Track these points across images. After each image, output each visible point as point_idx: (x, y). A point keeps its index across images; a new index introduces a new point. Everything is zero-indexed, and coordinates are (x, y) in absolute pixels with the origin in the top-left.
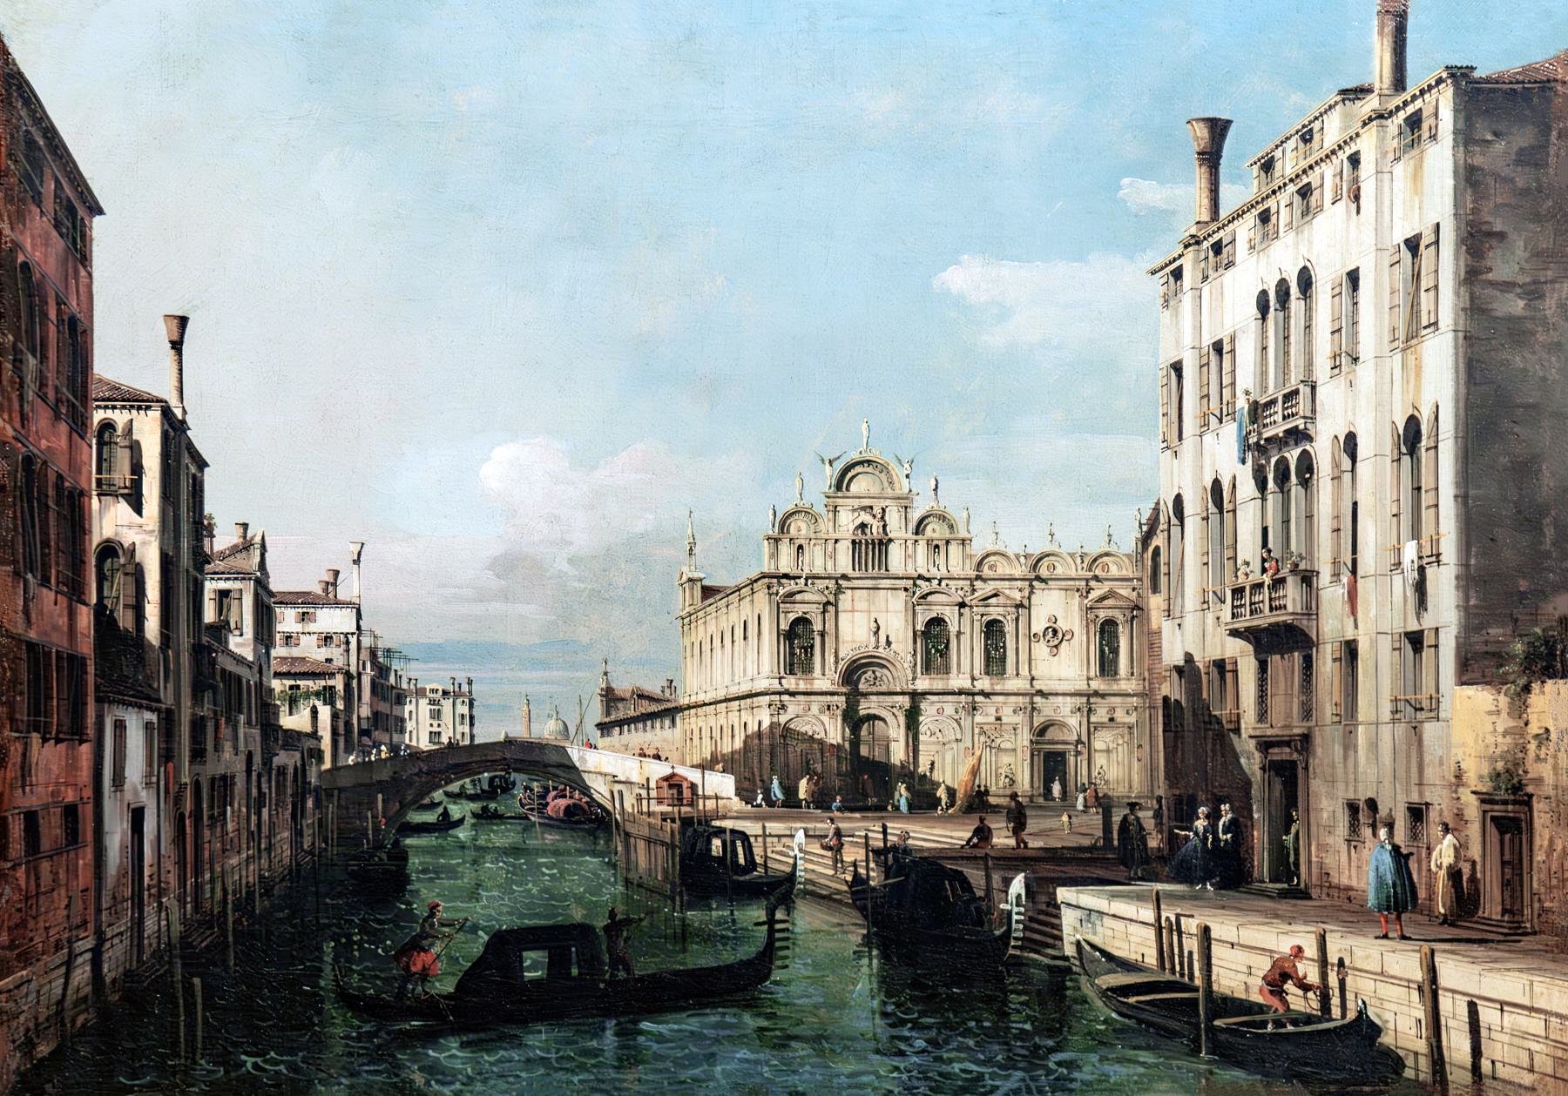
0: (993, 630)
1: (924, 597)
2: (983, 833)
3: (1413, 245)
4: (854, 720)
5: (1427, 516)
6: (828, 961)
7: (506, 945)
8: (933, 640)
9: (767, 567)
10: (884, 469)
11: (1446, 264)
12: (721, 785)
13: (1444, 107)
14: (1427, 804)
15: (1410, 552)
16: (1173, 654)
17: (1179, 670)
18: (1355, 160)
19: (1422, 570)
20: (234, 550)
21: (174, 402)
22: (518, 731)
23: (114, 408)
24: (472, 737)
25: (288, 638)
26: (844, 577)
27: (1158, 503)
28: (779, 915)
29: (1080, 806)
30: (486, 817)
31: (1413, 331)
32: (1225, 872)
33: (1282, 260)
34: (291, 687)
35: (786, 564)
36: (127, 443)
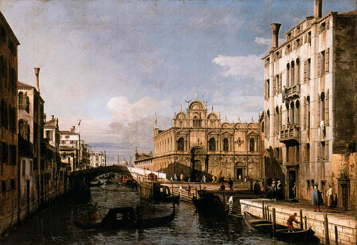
0: (225, 141)
2: (223, 187)
3: (323, 53)
6: (188, 218)
7: (113, 212)
8: (212, 143)
10: (200, 104)
11: (331, 57)
12: (163, 176)
15: (322, 123)
19: (325, 127)
21: (36, 88)
22: (116, 163)
26: (191, 128)
30: (108, 183)
32: (279, 197)
33: (293, 56)
34: (64, 153)
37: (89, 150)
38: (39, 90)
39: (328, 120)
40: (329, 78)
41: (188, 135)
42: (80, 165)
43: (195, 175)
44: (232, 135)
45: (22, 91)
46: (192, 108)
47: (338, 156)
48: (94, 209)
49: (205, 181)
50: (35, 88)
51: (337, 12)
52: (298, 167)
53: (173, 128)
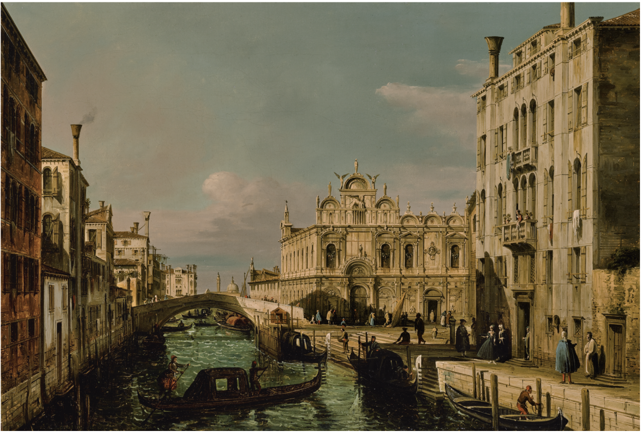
0: (408, 250)
1: (380, 235)
2: (406, 336)
3: (578, 91)
4: (353, 289)
5: (582, 200)
6: (340, 390)
7: (206, 377)
8: (385, 254)
9: (317, 223)
10: (363, 181)
11: (590, 99)
12: (298, 313)
13: (589, 37)
14: (583, 318)
15: (576, 213)
16: (480, 255)
17: (482, 260)
18: (553, 57)
19: (581, 220)
20: (97, 213)
21: (74, 159)
22: (214, 290)
23: (51, 161)
24: (195, 291)
25: (120, 252)
26: (349, 227)
27: (475, 193)
28: (322, 365)
29: (442, 323)
30: (198, 325)
31: (576, 127)
32: (502, 353)
33: (524, 97)
34: (120, 272)
35: (326, 221)
36: (55, 175)
37: (164, 265)
38: (79, 162)
39: (586, 209)
40: (588, 133)
41: (344, 239)
42: (148, 295)
43: (355, 314)
44: (421, 238)
45: (50, 166)
46: (350, 188)
47: (603, 274)
48: (166, 371)
49: (372, 323)
50: (71, 158)
51: (603, 18)
52: (532, 294)
53: (316, 227)
